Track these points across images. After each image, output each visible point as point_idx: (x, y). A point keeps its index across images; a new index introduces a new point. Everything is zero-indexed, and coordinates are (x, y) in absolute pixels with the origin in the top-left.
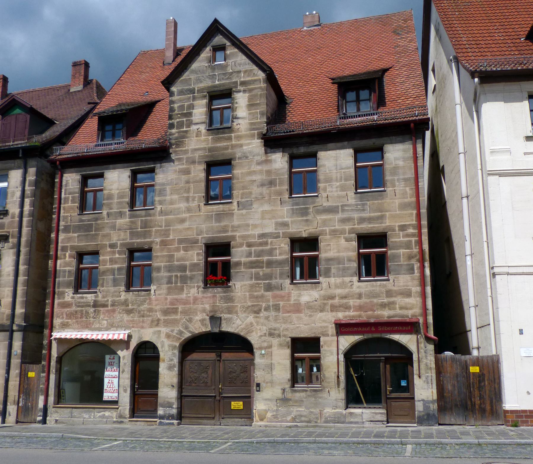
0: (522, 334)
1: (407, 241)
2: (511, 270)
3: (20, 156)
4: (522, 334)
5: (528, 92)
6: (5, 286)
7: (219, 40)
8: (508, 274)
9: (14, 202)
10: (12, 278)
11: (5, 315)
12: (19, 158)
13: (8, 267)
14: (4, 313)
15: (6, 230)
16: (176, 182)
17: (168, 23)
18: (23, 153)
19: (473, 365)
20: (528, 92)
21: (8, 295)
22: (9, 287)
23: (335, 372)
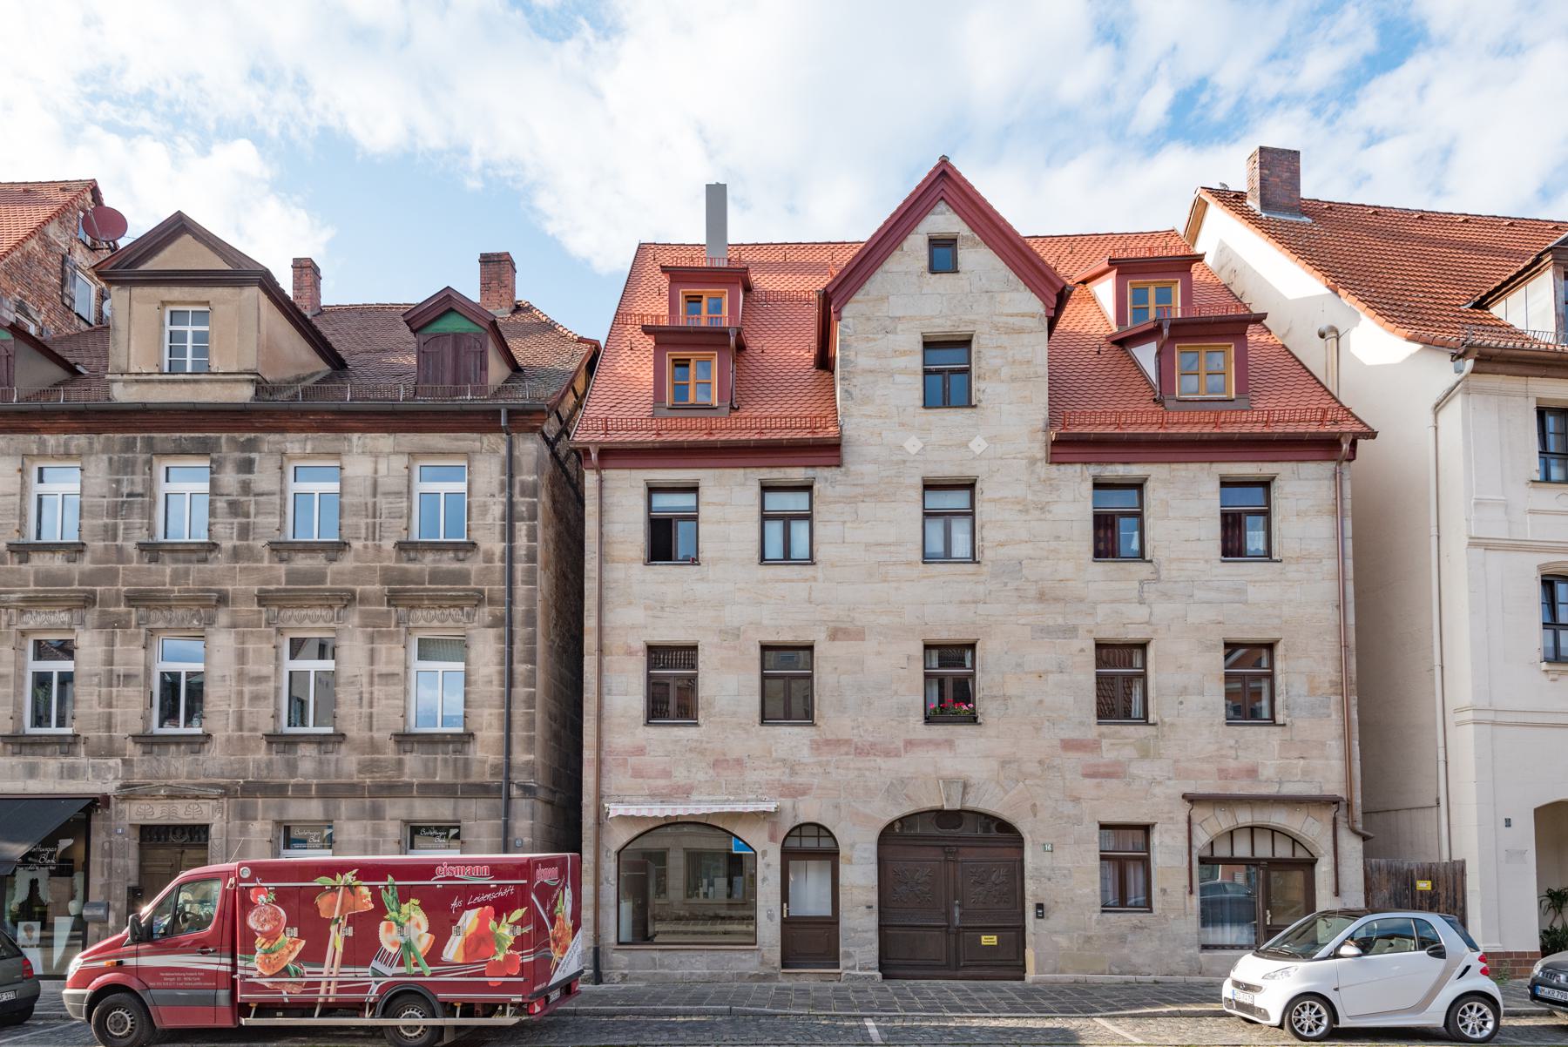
0: (486, 260)
1: (1307, 673)
2: (1502, 718)
3: (1239, 685)
4: (486, 260)
5: (1538, 399)
6: (482, 706)
7: (943, 221)
8: (1494, 723)
9: (490, 527)
10: (496, 689)
11: (487, 767)
12: (499, 430)
13: (486, 665)
14: (485, 762)
15: (472, 586)
16: (865, 517)
17: (964, 329)
18: (509, 420)
19: (1422, 879)
20: (1538, 399)
21: (490, 725)
22: (491, 707)
23: (1252, 773)
